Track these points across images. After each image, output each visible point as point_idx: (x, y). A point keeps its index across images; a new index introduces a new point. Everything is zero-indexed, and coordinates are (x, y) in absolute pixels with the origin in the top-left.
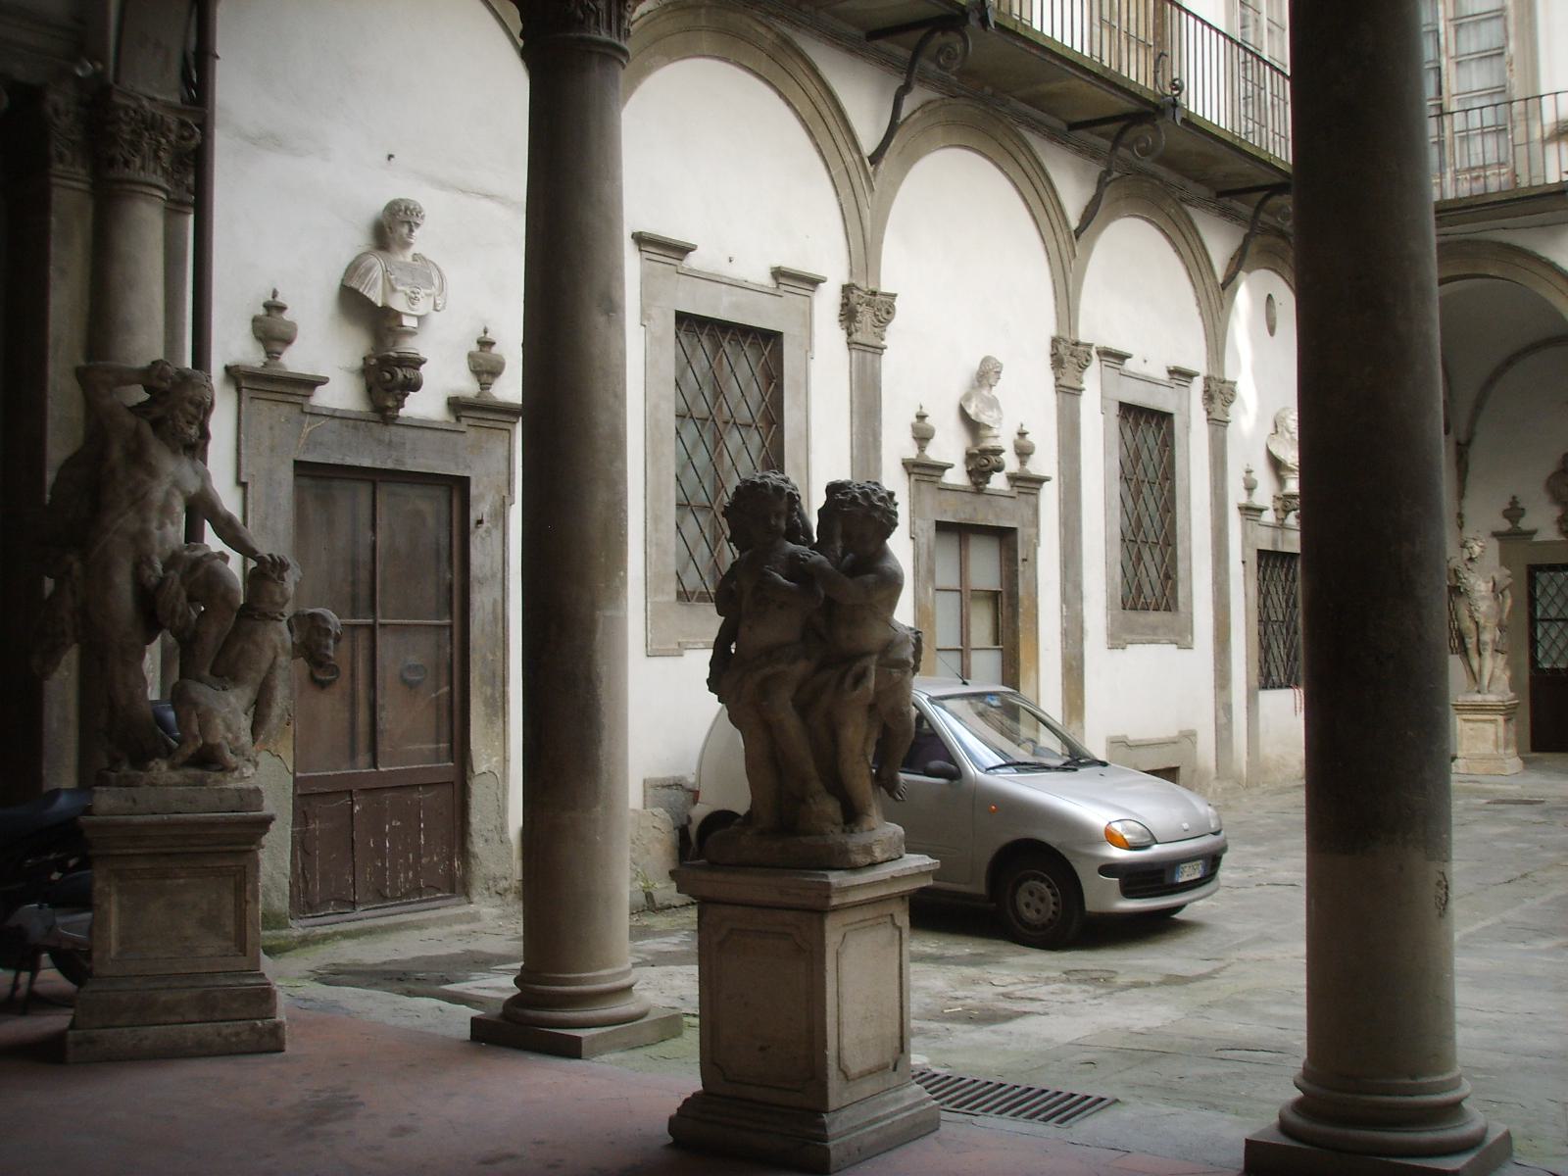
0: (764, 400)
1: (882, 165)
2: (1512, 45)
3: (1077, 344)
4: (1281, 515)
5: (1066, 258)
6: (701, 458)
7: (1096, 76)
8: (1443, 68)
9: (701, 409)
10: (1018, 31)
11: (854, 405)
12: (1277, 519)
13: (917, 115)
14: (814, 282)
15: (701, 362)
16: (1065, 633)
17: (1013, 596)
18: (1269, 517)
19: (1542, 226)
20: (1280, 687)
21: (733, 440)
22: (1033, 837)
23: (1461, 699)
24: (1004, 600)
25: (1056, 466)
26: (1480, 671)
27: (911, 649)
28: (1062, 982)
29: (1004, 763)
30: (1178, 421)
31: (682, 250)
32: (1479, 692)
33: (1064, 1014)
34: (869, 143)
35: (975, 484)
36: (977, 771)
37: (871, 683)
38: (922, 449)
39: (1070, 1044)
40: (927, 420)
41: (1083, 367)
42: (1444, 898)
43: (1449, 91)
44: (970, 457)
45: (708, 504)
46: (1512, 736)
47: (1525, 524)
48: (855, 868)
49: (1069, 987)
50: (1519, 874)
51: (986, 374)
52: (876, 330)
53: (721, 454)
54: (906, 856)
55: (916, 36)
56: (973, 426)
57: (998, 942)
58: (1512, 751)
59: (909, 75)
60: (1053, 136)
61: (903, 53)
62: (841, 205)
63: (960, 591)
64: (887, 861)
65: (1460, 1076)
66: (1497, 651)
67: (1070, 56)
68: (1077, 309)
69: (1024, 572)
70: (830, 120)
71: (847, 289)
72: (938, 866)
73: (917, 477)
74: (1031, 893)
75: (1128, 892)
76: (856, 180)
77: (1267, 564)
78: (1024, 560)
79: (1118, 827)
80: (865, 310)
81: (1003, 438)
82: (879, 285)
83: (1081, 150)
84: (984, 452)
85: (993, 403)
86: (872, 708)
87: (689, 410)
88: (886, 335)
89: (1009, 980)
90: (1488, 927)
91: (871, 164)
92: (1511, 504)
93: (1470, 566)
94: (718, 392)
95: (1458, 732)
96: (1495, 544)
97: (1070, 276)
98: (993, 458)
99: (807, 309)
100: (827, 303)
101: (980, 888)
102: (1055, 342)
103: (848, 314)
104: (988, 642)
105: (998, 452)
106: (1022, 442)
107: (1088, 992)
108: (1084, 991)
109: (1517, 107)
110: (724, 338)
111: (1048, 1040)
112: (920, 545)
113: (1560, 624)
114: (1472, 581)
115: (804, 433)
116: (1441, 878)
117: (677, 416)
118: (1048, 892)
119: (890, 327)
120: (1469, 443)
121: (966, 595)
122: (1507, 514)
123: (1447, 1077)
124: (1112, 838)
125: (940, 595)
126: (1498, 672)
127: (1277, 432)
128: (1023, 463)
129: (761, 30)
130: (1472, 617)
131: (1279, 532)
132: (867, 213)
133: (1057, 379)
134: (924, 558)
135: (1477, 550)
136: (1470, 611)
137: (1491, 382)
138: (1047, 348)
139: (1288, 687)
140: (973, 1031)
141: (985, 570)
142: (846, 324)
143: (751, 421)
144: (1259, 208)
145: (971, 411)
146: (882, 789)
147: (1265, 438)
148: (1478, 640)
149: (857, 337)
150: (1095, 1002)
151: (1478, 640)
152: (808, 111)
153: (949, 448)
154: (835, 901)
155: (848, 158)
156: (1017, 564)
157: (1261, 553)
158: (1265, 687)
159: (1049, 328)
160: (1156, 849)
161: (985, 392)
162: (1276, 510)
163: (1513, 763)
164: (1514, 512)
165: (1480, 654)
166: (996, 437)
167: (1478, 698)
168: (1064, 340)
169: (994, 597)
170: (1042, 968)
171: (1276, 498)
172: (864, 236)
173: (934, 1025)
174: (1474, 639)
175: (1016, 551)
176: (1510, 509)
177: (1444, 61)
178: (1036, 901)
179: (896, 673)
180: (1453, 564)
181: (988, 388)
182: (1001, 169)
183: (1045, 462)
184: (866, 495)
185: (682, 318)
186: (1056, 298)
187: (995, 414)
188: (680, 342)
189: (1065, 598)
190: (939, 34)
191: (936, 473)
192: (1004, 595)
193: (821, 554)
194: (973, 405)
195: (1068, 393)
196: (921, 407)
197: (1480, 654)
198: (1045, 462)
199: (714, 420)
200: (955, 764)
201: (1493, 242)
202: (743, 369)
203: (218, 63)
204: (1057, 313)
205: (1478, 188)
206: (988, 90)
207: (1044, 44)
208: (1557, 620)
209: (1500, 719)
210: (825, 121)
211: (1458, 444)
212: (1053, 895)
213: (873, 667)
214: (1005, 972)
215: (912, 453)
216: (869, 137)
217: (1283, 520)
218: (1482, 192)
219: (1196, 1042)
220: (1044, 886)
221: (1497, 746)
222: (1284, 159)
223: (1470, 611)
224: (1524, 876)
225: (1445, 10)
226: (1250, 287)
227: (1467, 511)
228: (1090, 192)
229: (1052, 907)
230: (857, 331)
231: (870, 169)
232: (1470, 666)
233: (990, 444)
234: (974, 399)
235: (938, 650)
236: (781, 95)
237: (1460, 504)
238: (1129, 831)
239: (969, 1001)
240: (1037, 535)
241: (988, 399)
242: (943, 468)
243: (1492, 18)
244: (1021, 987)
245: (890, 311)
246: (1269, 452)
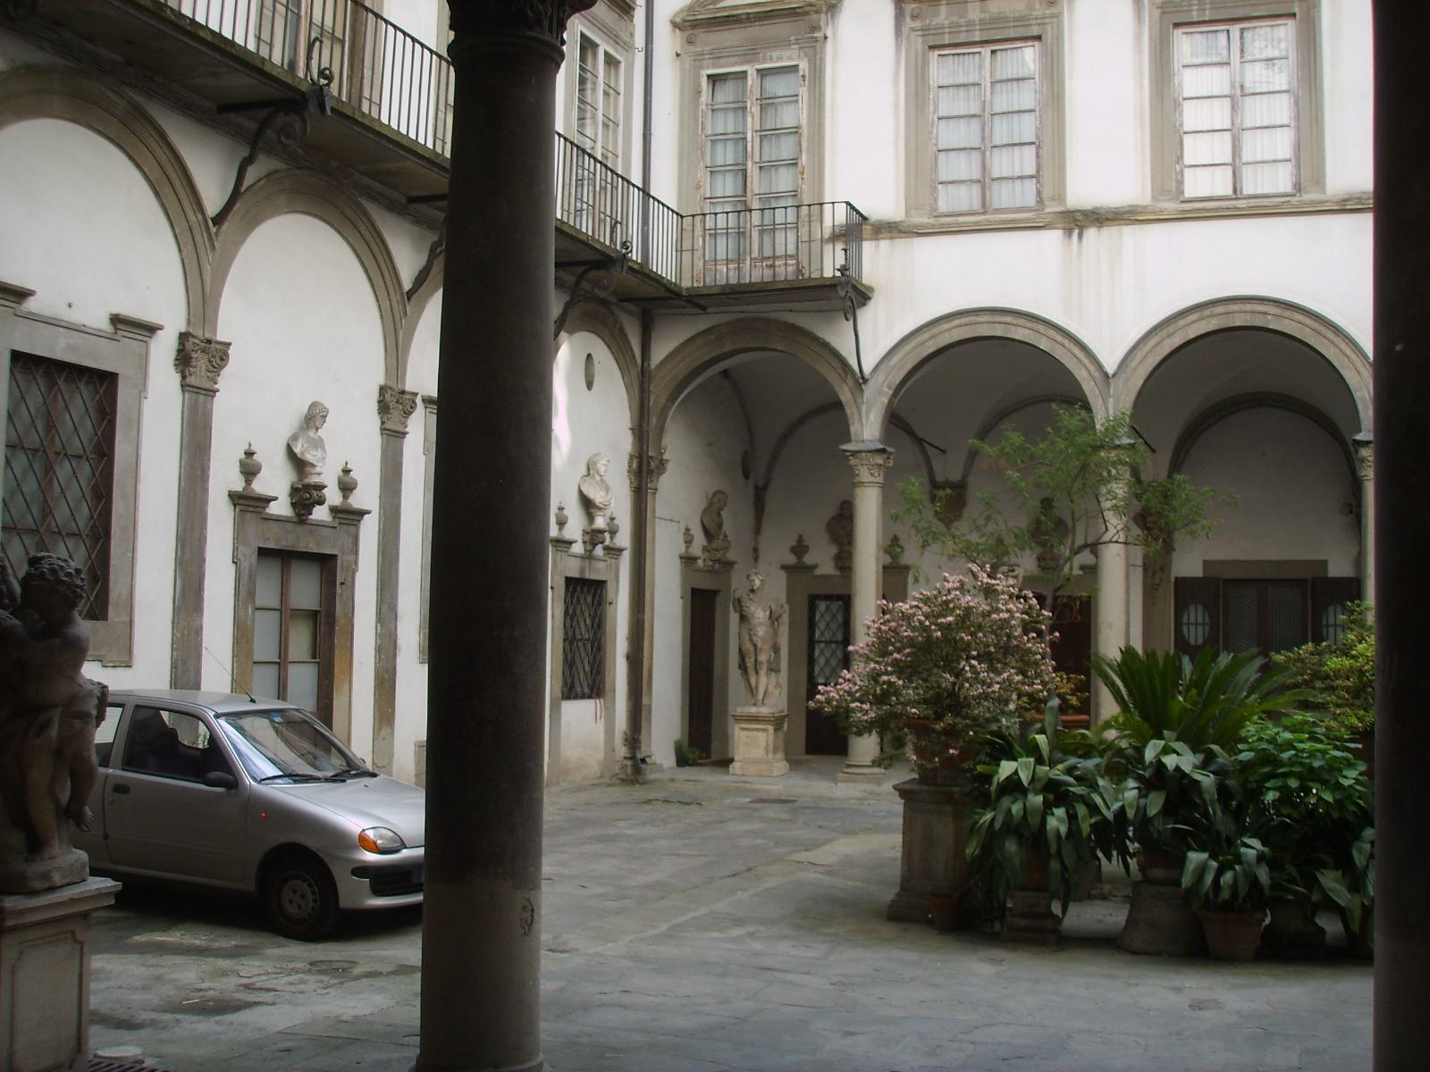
0: (96, 434)
1: (225, 226)
2: (804, 157)
3: (403, 392)
4: (589, 547)
5: (397, 318)
6: (30, 486)
7: (428, 160)
8: (749, 171)
9: (33, 440)
10: (356, 117)
11: (185, 441)
12: (585, 550)
13: (263, 182)
14: (151, 329)
15: (35, 398)
16: (379, 650)
17: (331, 615)
18: (578, 548)
19: (821, 311)
20: (583, 697)
21: (63, 470)
22: (297, 841)
23: (740, 711)
24: (322, 618)
25: (377, 501)
26: (757, 686)
27: (95, 702)
28: (303, 972)
29: (281, 773)
31: (21, 294)
32: (755, 705)
33: (290, 1003)
34: (213, 205)
35: (298, 515)
36: (252, 782)
37: (54, 732)
38: (248, 482)
39: (279, 1032)
40: (255, 457)
41: (408, 414)
42: (529, 920)
43: (752, 191)
44: (294, 491)
45: (34, 527)
46: (781, 743)
47: (808, 559)
48: (33, 893)
49: (308, 977)
50: (744, 868)
51: (314, 417)
52: (210, 374)
53: (50, 482)
54: (91, 879)
55: (262, 113)
56: (299, 464)
57: (264, 934)
58: (780, 755)
59: (255, 145)
60: (392, 207)
61: (252, 126)
62: (183, 260)
63: (280, 610)
64: (68, 885)
65: (541, 1063)
66: (771, 670)
67: (404, 142)
68: (405, 362)
69: (341, 594)
70: (177, 184)
71: (183, 337)
72: (120, 888)
73: (243, 508)
74: (294, 892)
75: (378, 891)
76: (198, 239)
77: (575, 589)
78: (342, 584)
79: (371, 834)
80: (200, 357)
81: (328, 476)
82: (215, 335)
83: (419, 220)
84: (308, 487)
85: (319, 444)
86: (58, 753)
87: (21, 441)
88: (220, 379)
89: (256, 971)
90: (694, 918)
91: (214, 225)
92: (798, 541)
93: (751, 596)
94: (51, 426)
95: (736, 738)
96: (783, 575)
97: (401, 333)
98: (315, 493)
99: (144, 353)
100: (163, 350)
101: (250, 886)
102: (382, 390)
103: (183, 360)
104: (306, 657)
105: (321, 487)
106: (346, 479)
107: (322, 982)
108: (319, 982)
109: (805, 210)
110: (59, 377)
111: (261, 1029)
112: (242, 568)
113: (833, 646)
114: (753, 609)
115: (134, 466)
116: (526, 904)
117: (7, 446)
118: (309, 890)
119: (223, 372)
120: (765, 487)
121: (287, 614)
122: (794, 550)
123: (534, 1063)
124: (364, 842)
125: (257, 612)
126: (771, 688)
127: (589, 474)
128: (345, 497)
129: (113, 97)
130: (751, 640)
131: (587, 562)
132: (207, 269)
133: (383, 423)
134: (245, 580)
135: (758, 582)
136: (750, 636)
137: (785, 437)
138: (375, 395)
139: (590, 697)
140: (199, 1022)
141: (305, 591)
142: (180, 368)
143: (82, 452)
144: (581, 277)
145: (297, 450)
146: (71, 821)
147: (577, 479)
148: (756, 660)
149: (191, 380)
150: (325, 991)
151: (756, 660)
152: (156, 173)
153: (275, 483)
154: (10, 923)
155: (192, 218)
156: (335, 587)
157: (569, 580)
158: (568, 698)
159: (379, 378)
160: (405, 853)
161: (311, 434)
162: (584, 542)
163: (781, 766)
164: (800, 549)
165: (757, 672)
166: (319, 474)
167: (753, 710)
168: (390, 388)
169: (313, 616)
170: (291, 959)
171: (585, 532)
172: (203, 289)
173: (167, 1017)
174: (753, 659)
175: (335, 575)
176: (798, 546)
177: (749, 164)
178: (297, 898)
179: (77, 723)
180: (737, 595)
181: (314, 430)
182: (342, 235)
183: (367, 496)
184: (53, 571)
185: (17, 357)
186: (386, 351)
187: (319, 453)
188: (15, 380)
189: (380, 618)
190: (282, 114)
191: (261, 505)
192: (323, 614)
193: (17, 618)
194: (300, 445)
195: (393, 436)
196: (250, 445)
197: (757, 672)
198: (367, 496)
199: (45, 451)
200: (234, 775)
201: (781, 322)
202: (77, 407)
203: (629, 425)
204: (386, 364)
205: (768, 275)
206: (334, 164)
207: (380, 130)
208: (831, 642)
209: (771, 728)
210: (172, 185)
211: (757, 488)
212: (313, 893)
213: (56, 719)
214: (257, 963)
215: (238, 485)
216: (213, 201)
217: (591, 551)
218: (771, 279)
219: (389, 1029)
220: (305, 885)
221: (767, 752)
222: (602, 240)
223: (750, 636)
224: (749, 870)
225: (753, 124)
226: (572, 348)
227: (762, 548)
228: (422, 260)
229: (312, 904)
230: (191, 375)
231: (213, 230)
232: (749, 683)
233: (314, 480)
234: (300, 440)
235: (255, 663)
236: (131, 158)
237: (756, 540)
238: (381, 837)
239: (211, 992)
240: (356, 562)
241: (313, 439)
242: (267, 500)
243: (791, 133)
244: (264, 978)
245: (224, 358)
246: (581, 492)
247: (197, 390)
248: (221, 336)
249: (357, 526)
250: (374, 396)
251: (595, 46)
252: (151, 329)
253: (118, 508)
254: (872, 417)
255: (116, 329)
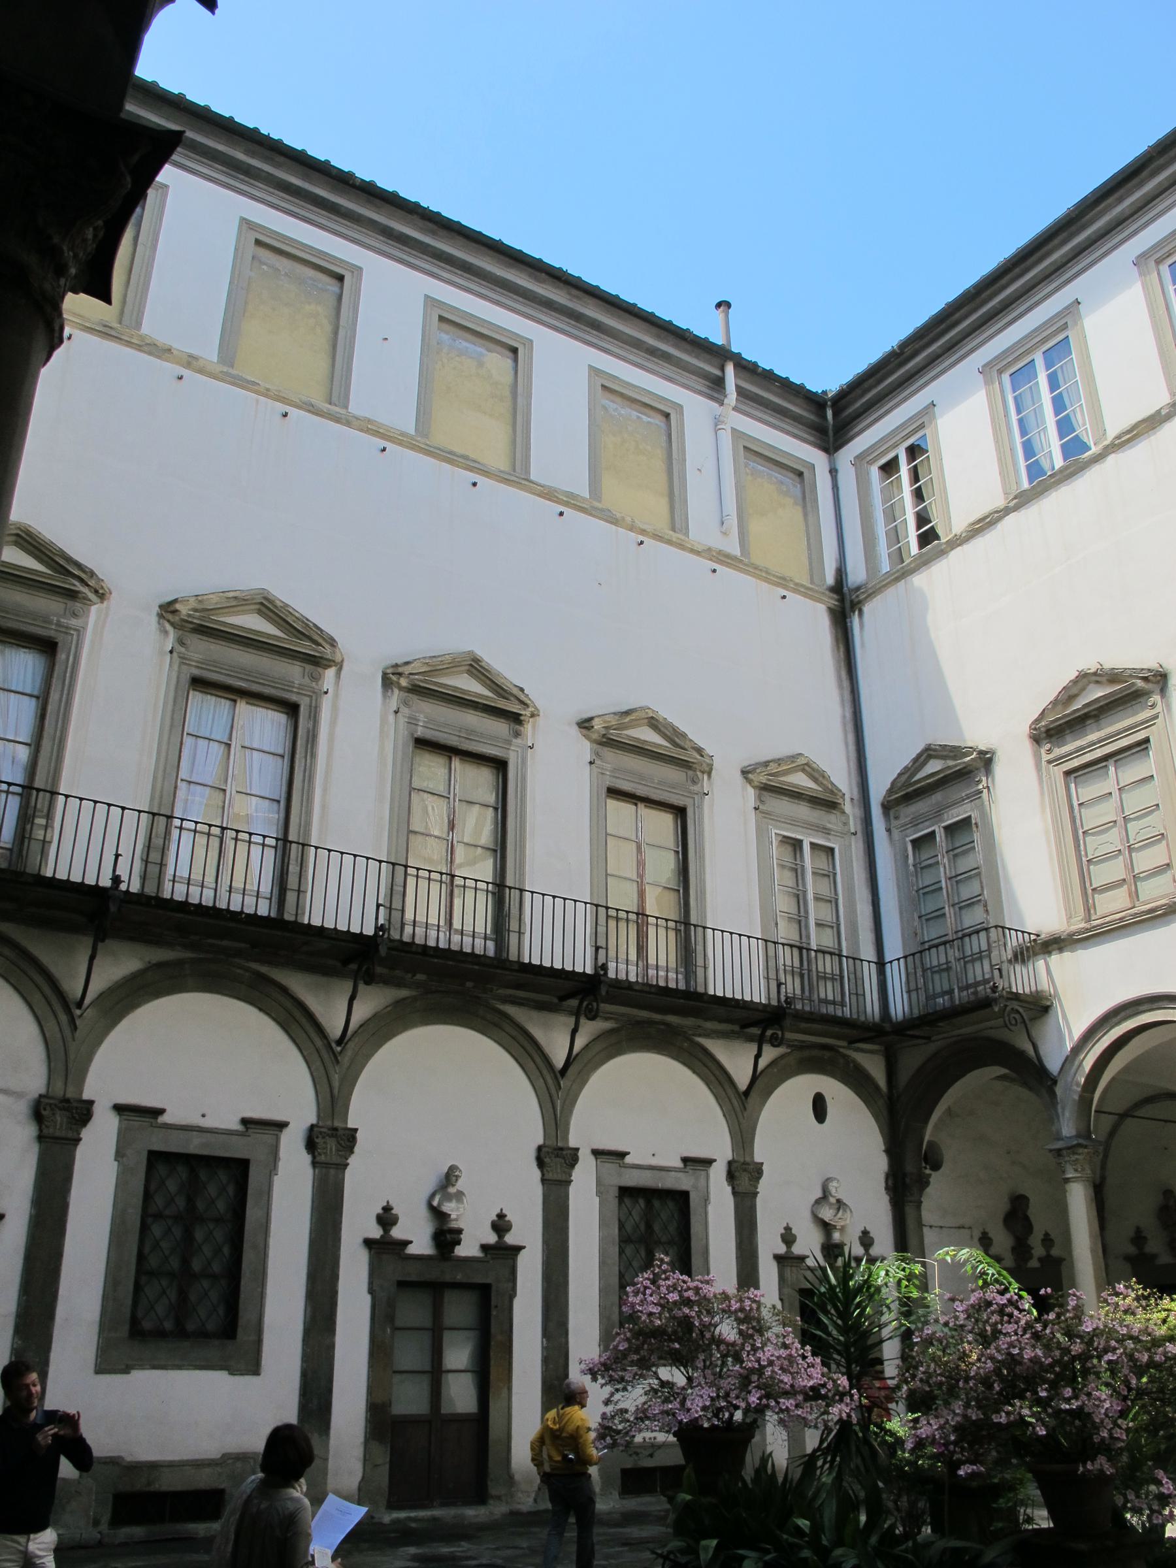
14: (708, 1162)
30: (693, 1196)
31: (622, 1155)
56: (438, 1215)
80: (744, 1175)
100: (718, 1173)
103: (731, 1176)
106: (501, 1222)
149: (318, 1159)
153: (809, 1244)
183: (528, 1233)
203: (883, 1148)
215: (782, 1249)
235: (394, 1372)
247: (327, 1165)
248: (757, 1159)
249: (516, 1255)
250: (532, 1154)
251: (801, 841)
252: (281, 1126)
253: (248, 1256)
254: (1067, 1114)
255: (247, 1129)
